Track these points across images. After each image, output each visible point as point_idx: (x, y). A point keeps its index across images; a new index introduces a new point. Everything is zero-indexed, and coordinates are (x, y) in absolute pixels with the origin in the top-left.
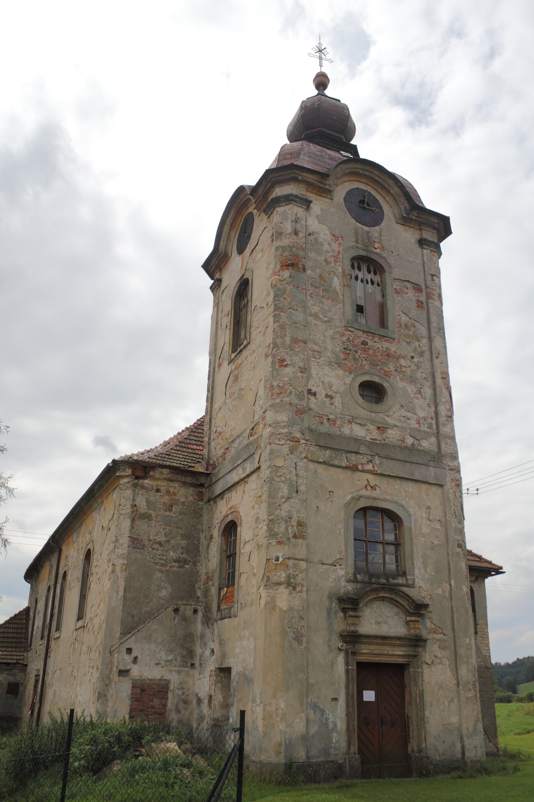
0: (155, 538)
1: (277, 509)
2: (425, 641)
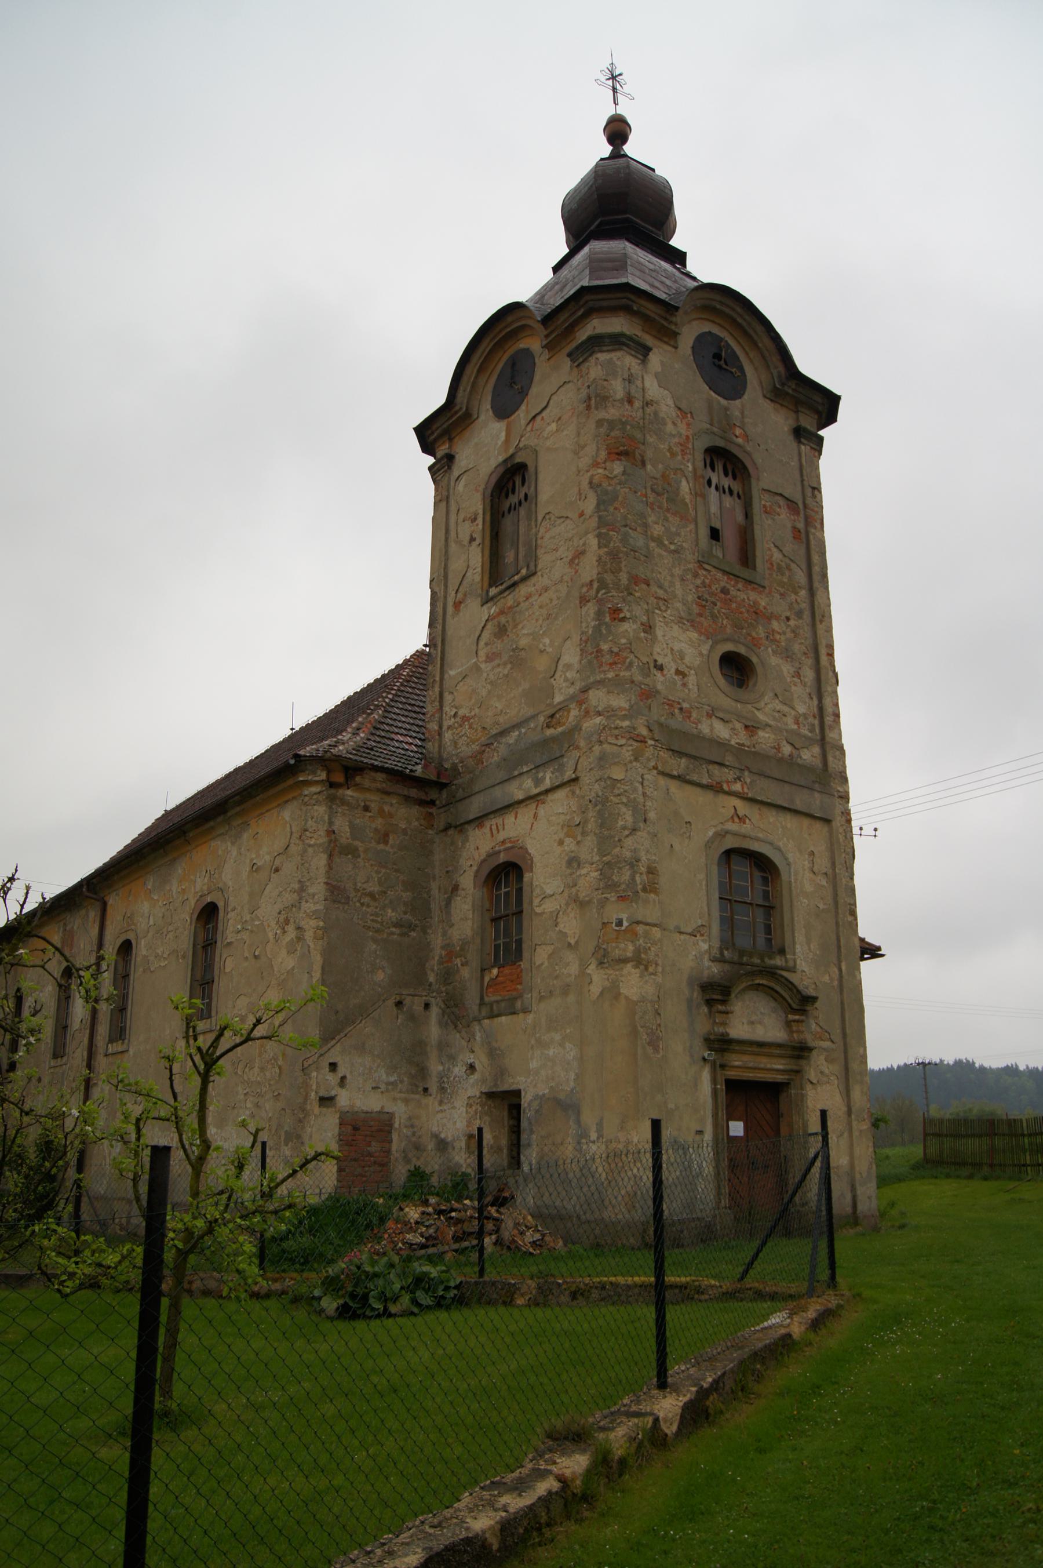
0: (364, 886)
1: (616, 846)
2: (810, 1049)
